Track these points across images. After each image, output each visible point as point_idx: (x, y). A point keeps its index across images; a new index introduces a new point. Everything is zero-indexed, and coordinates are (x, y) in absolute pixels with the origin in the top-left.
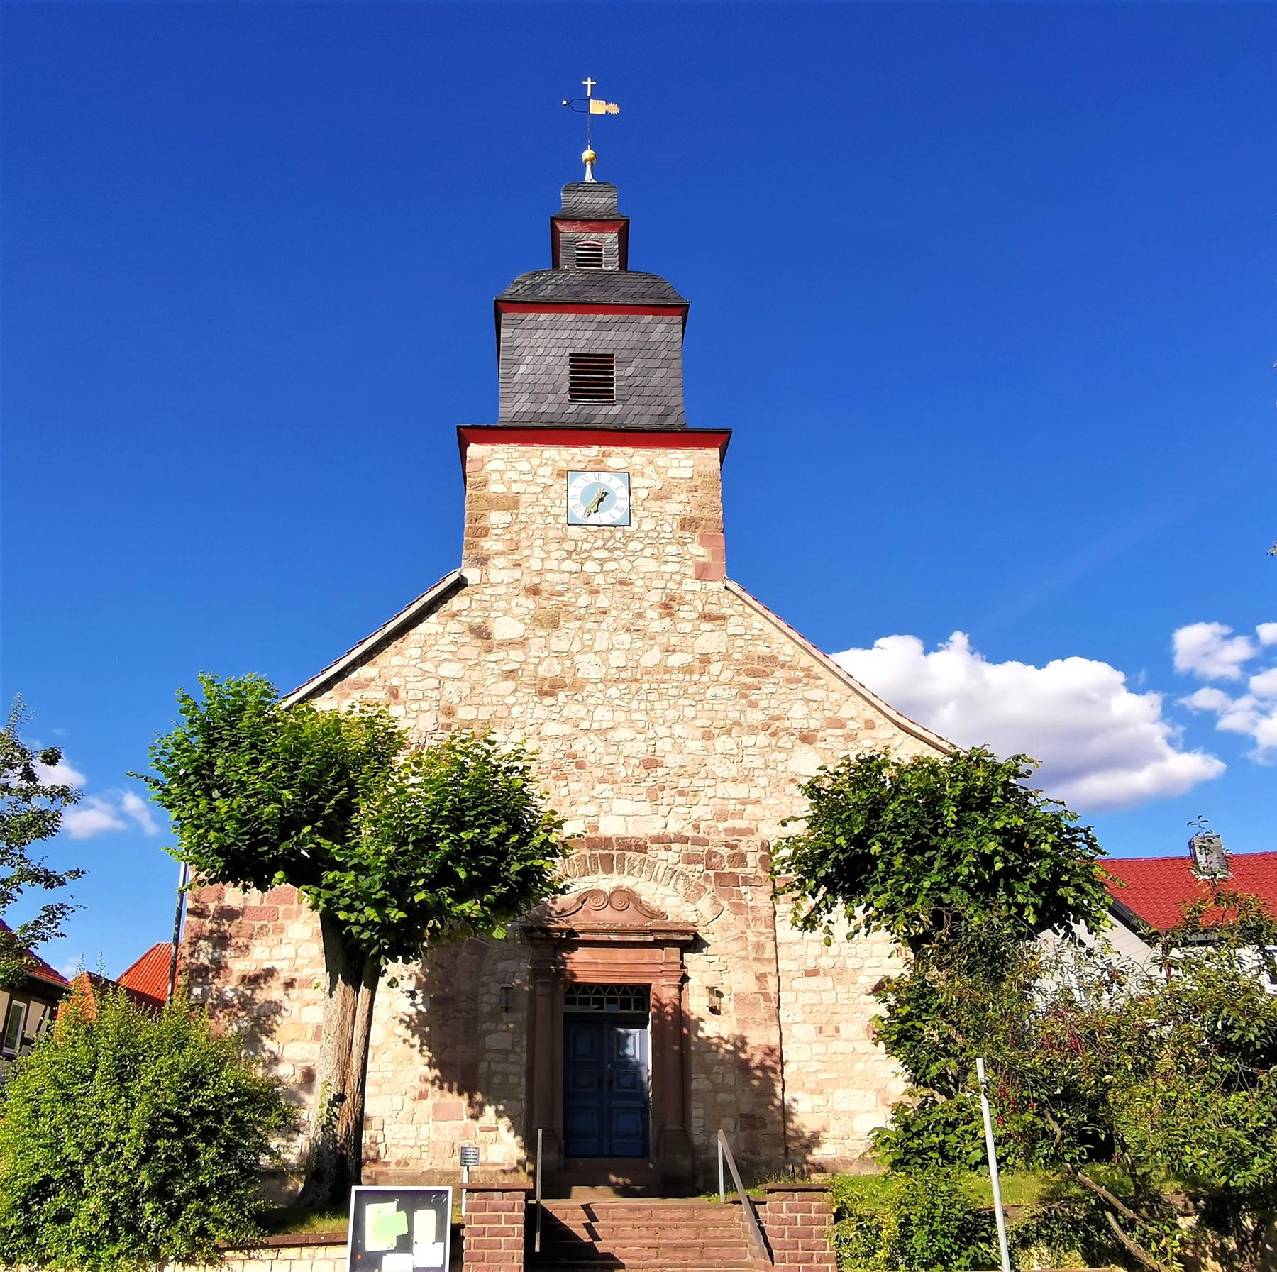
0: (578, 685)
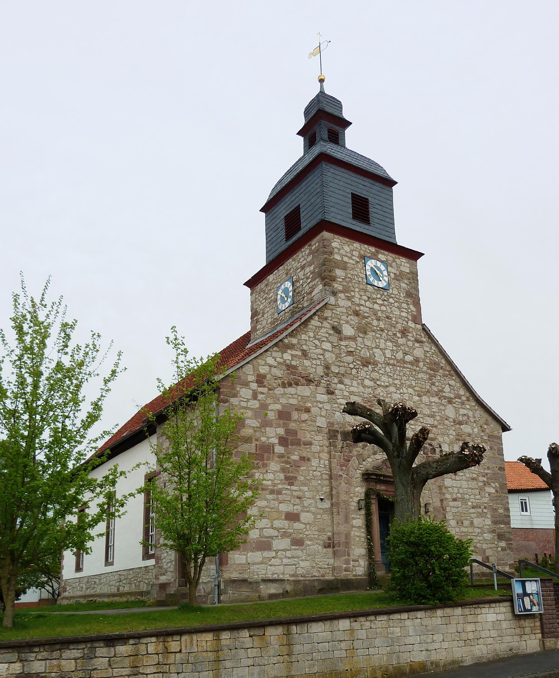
0: (375, 364)
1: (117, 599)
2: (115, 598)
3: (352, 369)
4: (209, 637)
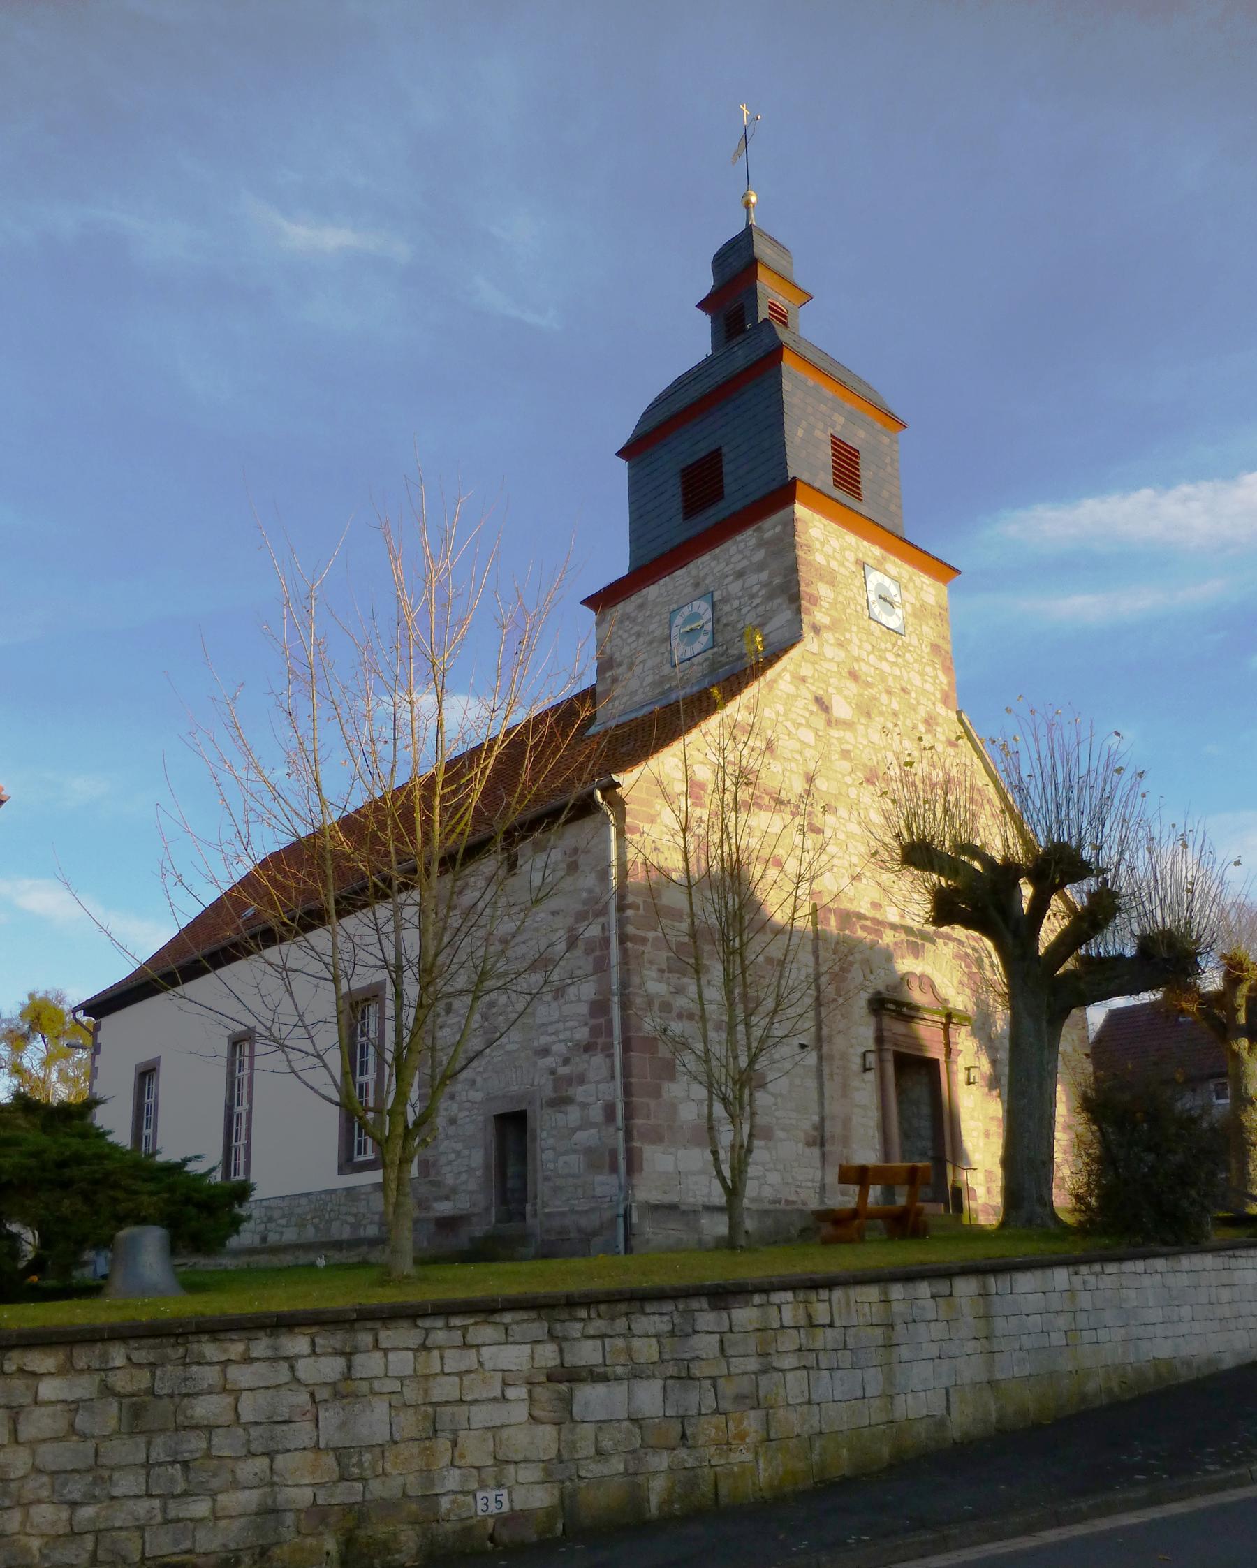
1: (262, 1260)
2: (256, 1258)
3: (849, 786)
4: (871, 1293)
